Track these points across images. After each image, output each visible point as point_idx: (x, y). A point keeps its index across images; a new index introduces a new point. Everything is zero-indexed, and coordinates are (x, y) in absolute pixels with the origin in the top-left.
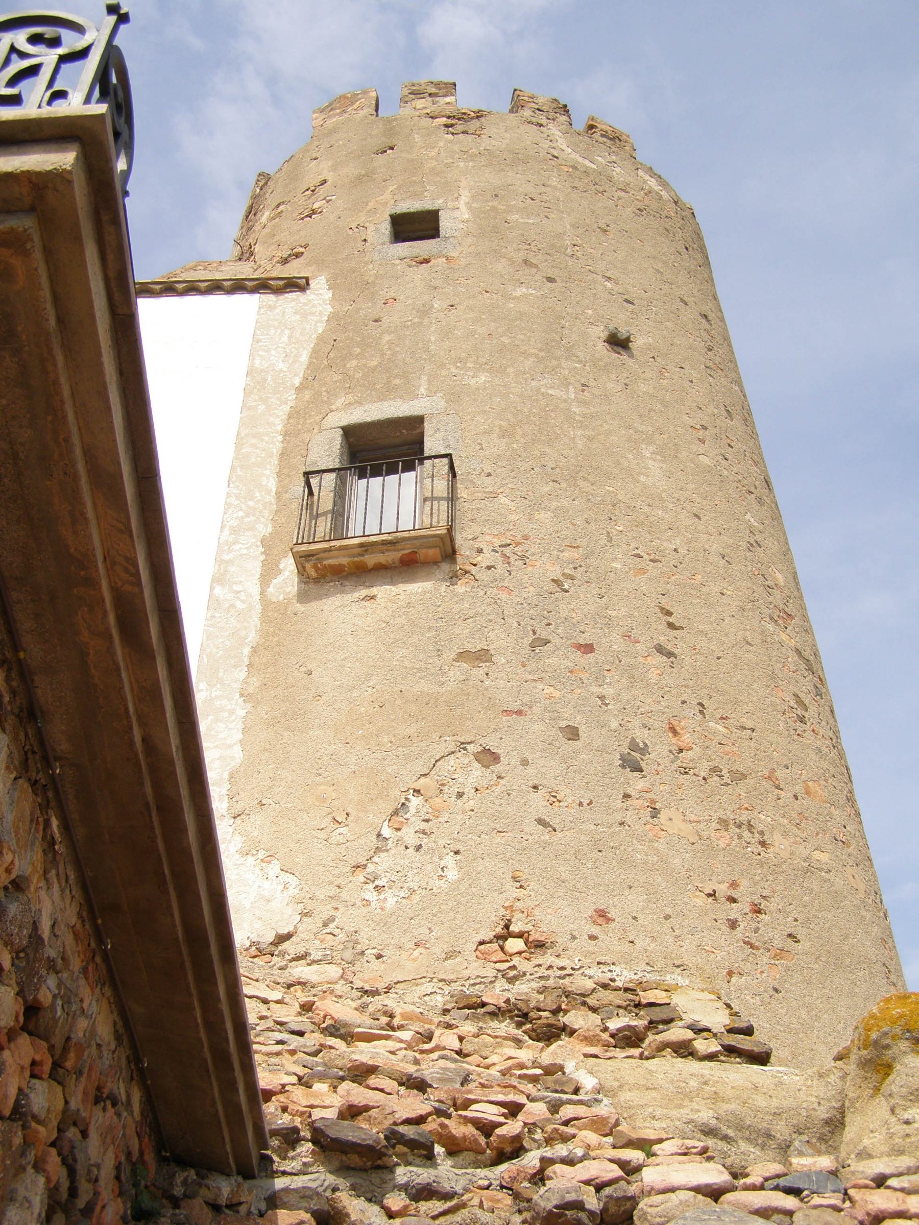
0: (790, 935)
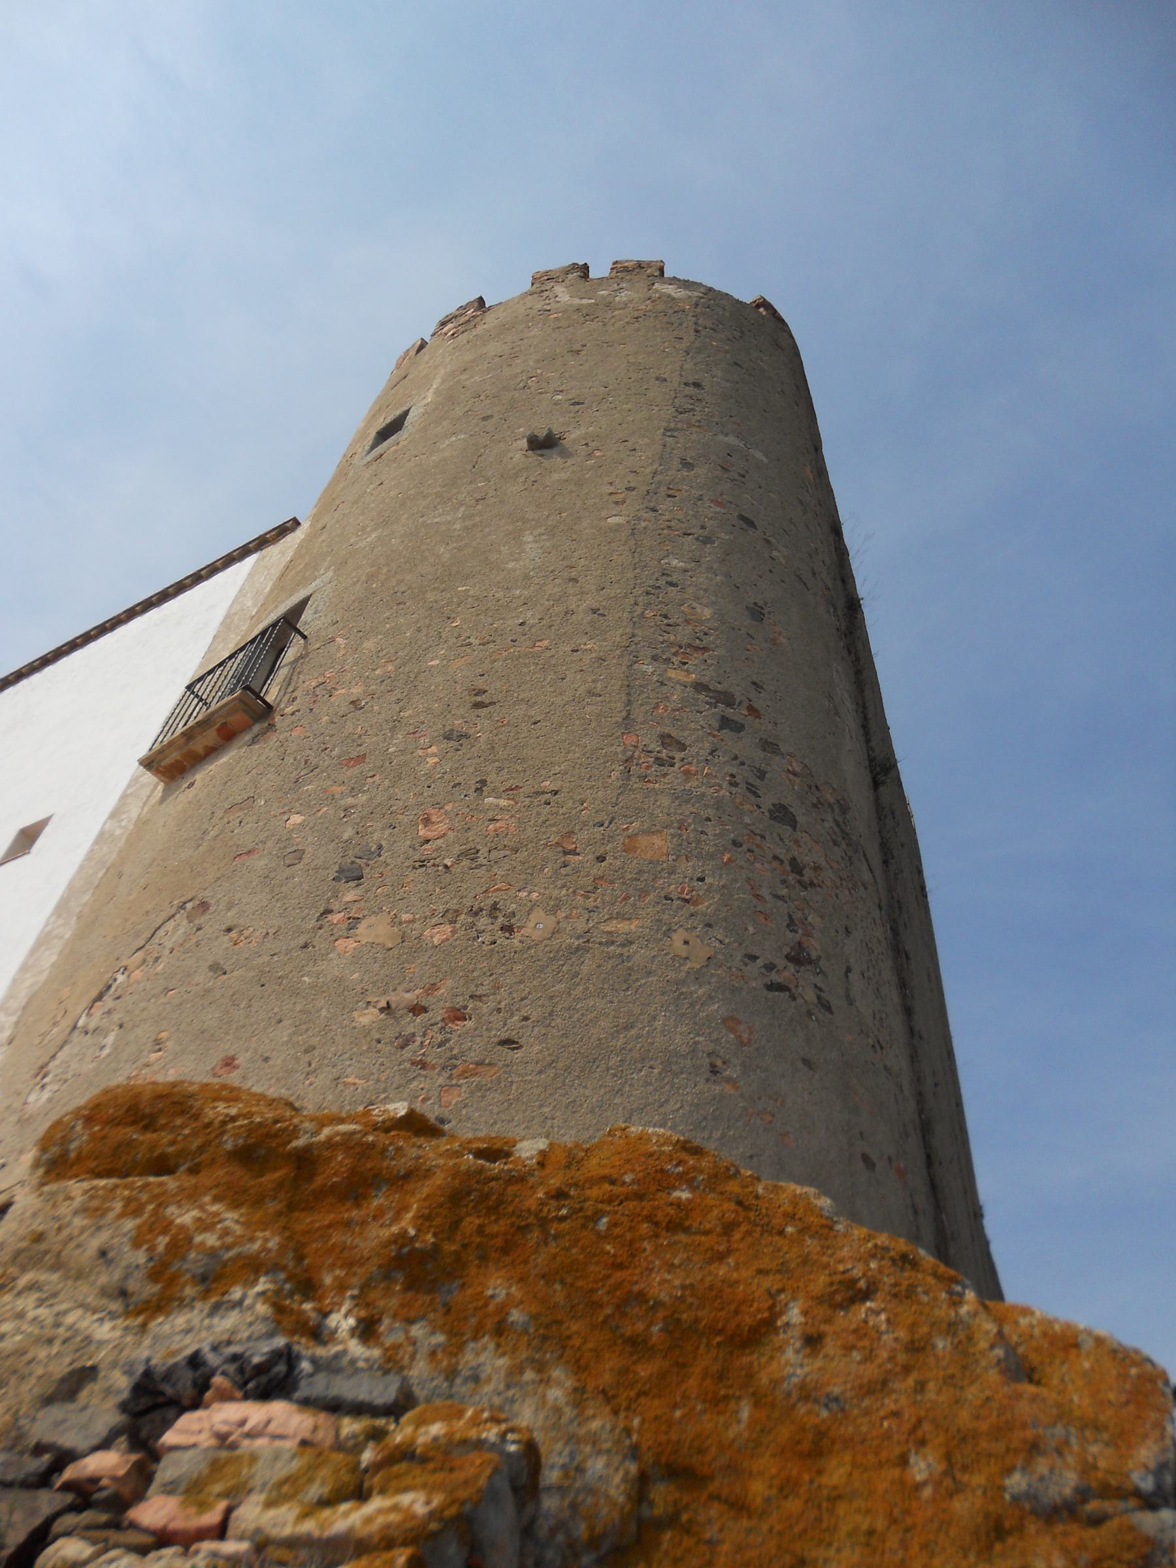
0: (503, 1043)
